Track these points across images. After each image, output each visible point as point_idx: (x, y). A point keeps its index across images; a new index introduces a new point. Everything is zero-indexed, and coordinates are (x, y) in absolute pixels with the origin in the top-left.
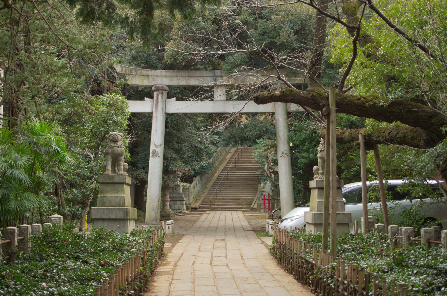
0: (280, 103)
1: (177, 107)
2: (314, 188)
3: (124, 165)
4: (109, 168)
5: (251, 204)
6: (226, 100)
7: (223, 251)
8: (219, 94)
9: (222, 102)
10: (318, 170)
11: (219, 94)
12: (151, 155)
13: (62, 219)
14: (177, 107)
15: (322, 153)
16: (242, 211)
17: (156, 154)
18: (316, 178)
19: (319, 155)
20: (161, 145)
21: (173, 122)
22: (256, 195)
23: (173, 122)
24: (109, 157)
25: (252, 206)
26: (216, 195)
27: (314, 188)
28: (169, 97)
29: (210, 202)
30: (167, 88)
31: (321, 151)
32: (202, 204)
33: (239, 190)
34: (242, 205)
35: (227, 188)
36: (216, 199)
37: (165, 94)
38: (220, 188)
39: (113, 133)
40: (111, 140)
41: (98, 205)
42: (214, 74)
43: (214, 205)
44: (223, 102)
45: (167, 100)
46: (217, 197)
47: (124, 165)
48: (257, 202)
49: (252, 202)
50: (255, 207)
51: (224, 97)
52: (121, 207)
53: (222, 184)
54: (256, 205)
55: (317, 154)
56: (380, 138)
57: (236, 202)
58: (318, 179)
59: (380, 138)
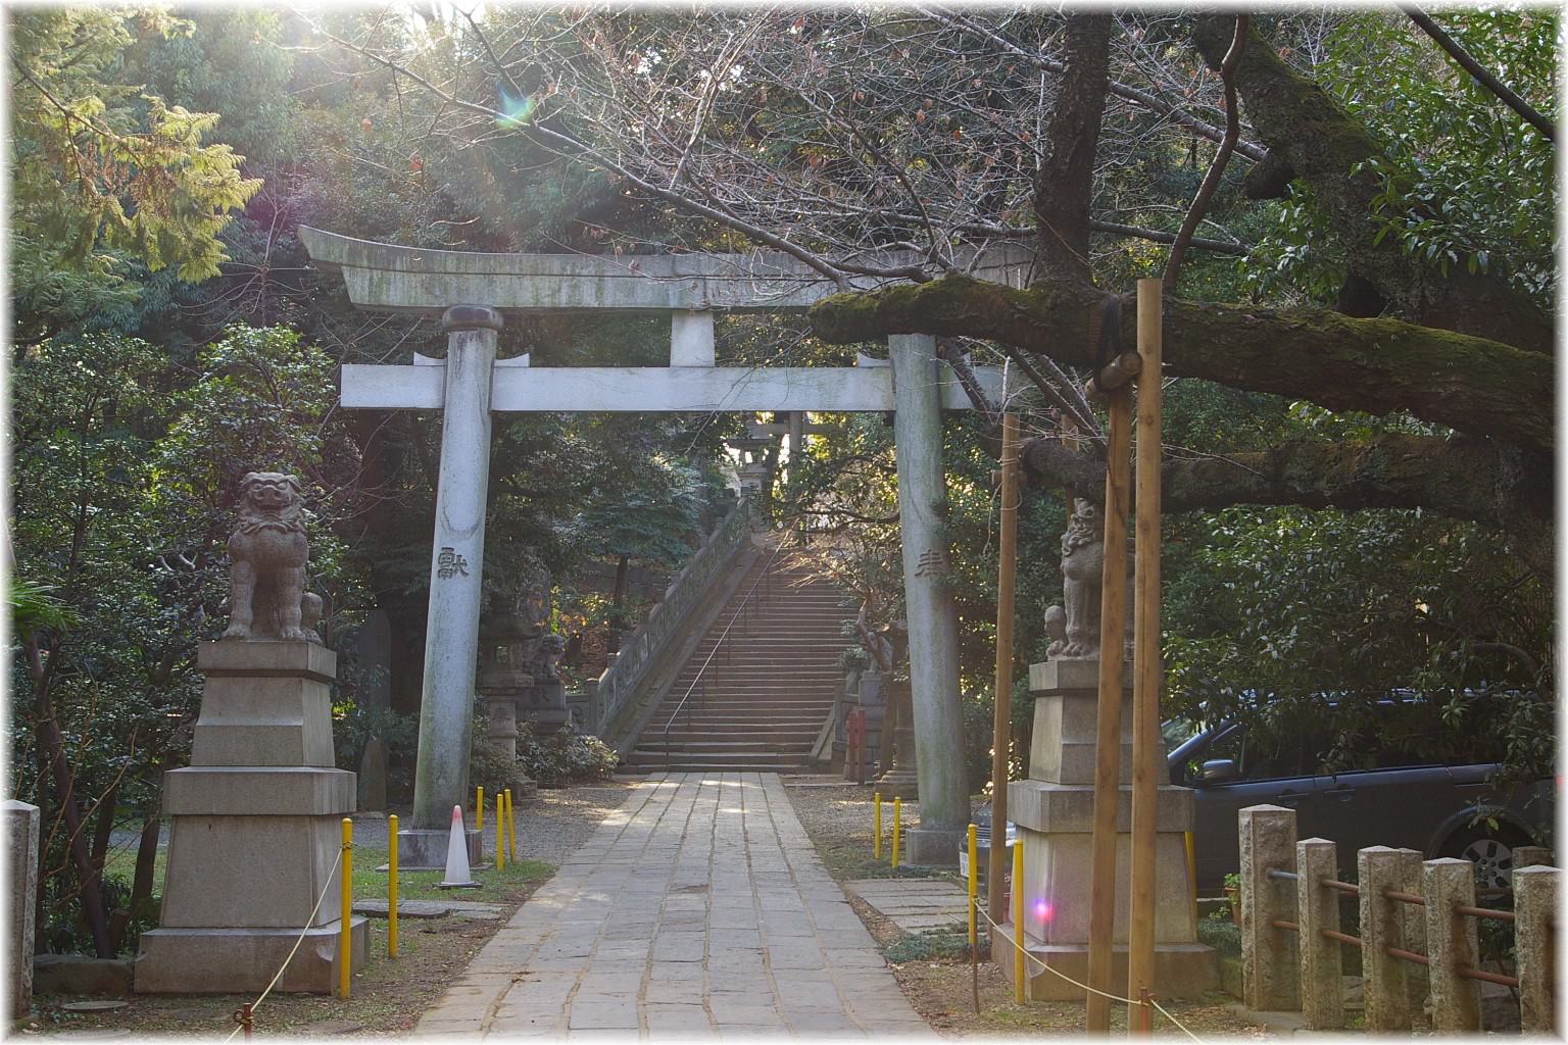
0: (915, 337)
1: (533, 388)
2: (1048, 694)
3: (305, 601)
4: (244, 611)
5: (810, 748)
6: (717, 365)
7: (694, 935)
8: (692, 341)
9: (700, 373)
10: (1062, 620)
11: (692, 341)
12: (435, 567)
13: (36, 817)
14: (533, 388)
15: (1079, 554)
16: (778, 771)
17: (453, 565)
18: (1054, 653)
19: (1066, 563)
20: (474, 528)
21: (514, 439)
22: (827, 713)
23: (514, 439)
24: (243, 568)
25: (814, 752)
26: (689, 714)
27: (1048, 694)
28: (507, 349)
29: (667, 738)
30: (498, 320)
31: (1074, 547)
32: (636, 748)
33: (771, 698)
34: (778, 750)
35: (726, 691)
36: (688, 729)
37: (491, 337)
38: (703, 692)
39: (264, 476)
40: (253, 503)
41: (194, 757)
42: (673, 269)
43: (680, 749)
44: (705, 371)
45: (498, 363)
46: (689, 721)
47: (305, 601)
48: (833, 734)
49: (815, 738)
50: (827, 755)
51: (709, 354)
52: (292, 770)
53: (708, 677)
54: (828, 749)
55: (1058, 559)
56: (1322, 484)
57: (757, 739)
58: (1065, 658)
59: (1322, 484)
